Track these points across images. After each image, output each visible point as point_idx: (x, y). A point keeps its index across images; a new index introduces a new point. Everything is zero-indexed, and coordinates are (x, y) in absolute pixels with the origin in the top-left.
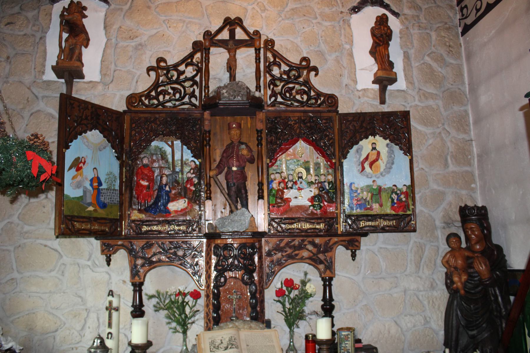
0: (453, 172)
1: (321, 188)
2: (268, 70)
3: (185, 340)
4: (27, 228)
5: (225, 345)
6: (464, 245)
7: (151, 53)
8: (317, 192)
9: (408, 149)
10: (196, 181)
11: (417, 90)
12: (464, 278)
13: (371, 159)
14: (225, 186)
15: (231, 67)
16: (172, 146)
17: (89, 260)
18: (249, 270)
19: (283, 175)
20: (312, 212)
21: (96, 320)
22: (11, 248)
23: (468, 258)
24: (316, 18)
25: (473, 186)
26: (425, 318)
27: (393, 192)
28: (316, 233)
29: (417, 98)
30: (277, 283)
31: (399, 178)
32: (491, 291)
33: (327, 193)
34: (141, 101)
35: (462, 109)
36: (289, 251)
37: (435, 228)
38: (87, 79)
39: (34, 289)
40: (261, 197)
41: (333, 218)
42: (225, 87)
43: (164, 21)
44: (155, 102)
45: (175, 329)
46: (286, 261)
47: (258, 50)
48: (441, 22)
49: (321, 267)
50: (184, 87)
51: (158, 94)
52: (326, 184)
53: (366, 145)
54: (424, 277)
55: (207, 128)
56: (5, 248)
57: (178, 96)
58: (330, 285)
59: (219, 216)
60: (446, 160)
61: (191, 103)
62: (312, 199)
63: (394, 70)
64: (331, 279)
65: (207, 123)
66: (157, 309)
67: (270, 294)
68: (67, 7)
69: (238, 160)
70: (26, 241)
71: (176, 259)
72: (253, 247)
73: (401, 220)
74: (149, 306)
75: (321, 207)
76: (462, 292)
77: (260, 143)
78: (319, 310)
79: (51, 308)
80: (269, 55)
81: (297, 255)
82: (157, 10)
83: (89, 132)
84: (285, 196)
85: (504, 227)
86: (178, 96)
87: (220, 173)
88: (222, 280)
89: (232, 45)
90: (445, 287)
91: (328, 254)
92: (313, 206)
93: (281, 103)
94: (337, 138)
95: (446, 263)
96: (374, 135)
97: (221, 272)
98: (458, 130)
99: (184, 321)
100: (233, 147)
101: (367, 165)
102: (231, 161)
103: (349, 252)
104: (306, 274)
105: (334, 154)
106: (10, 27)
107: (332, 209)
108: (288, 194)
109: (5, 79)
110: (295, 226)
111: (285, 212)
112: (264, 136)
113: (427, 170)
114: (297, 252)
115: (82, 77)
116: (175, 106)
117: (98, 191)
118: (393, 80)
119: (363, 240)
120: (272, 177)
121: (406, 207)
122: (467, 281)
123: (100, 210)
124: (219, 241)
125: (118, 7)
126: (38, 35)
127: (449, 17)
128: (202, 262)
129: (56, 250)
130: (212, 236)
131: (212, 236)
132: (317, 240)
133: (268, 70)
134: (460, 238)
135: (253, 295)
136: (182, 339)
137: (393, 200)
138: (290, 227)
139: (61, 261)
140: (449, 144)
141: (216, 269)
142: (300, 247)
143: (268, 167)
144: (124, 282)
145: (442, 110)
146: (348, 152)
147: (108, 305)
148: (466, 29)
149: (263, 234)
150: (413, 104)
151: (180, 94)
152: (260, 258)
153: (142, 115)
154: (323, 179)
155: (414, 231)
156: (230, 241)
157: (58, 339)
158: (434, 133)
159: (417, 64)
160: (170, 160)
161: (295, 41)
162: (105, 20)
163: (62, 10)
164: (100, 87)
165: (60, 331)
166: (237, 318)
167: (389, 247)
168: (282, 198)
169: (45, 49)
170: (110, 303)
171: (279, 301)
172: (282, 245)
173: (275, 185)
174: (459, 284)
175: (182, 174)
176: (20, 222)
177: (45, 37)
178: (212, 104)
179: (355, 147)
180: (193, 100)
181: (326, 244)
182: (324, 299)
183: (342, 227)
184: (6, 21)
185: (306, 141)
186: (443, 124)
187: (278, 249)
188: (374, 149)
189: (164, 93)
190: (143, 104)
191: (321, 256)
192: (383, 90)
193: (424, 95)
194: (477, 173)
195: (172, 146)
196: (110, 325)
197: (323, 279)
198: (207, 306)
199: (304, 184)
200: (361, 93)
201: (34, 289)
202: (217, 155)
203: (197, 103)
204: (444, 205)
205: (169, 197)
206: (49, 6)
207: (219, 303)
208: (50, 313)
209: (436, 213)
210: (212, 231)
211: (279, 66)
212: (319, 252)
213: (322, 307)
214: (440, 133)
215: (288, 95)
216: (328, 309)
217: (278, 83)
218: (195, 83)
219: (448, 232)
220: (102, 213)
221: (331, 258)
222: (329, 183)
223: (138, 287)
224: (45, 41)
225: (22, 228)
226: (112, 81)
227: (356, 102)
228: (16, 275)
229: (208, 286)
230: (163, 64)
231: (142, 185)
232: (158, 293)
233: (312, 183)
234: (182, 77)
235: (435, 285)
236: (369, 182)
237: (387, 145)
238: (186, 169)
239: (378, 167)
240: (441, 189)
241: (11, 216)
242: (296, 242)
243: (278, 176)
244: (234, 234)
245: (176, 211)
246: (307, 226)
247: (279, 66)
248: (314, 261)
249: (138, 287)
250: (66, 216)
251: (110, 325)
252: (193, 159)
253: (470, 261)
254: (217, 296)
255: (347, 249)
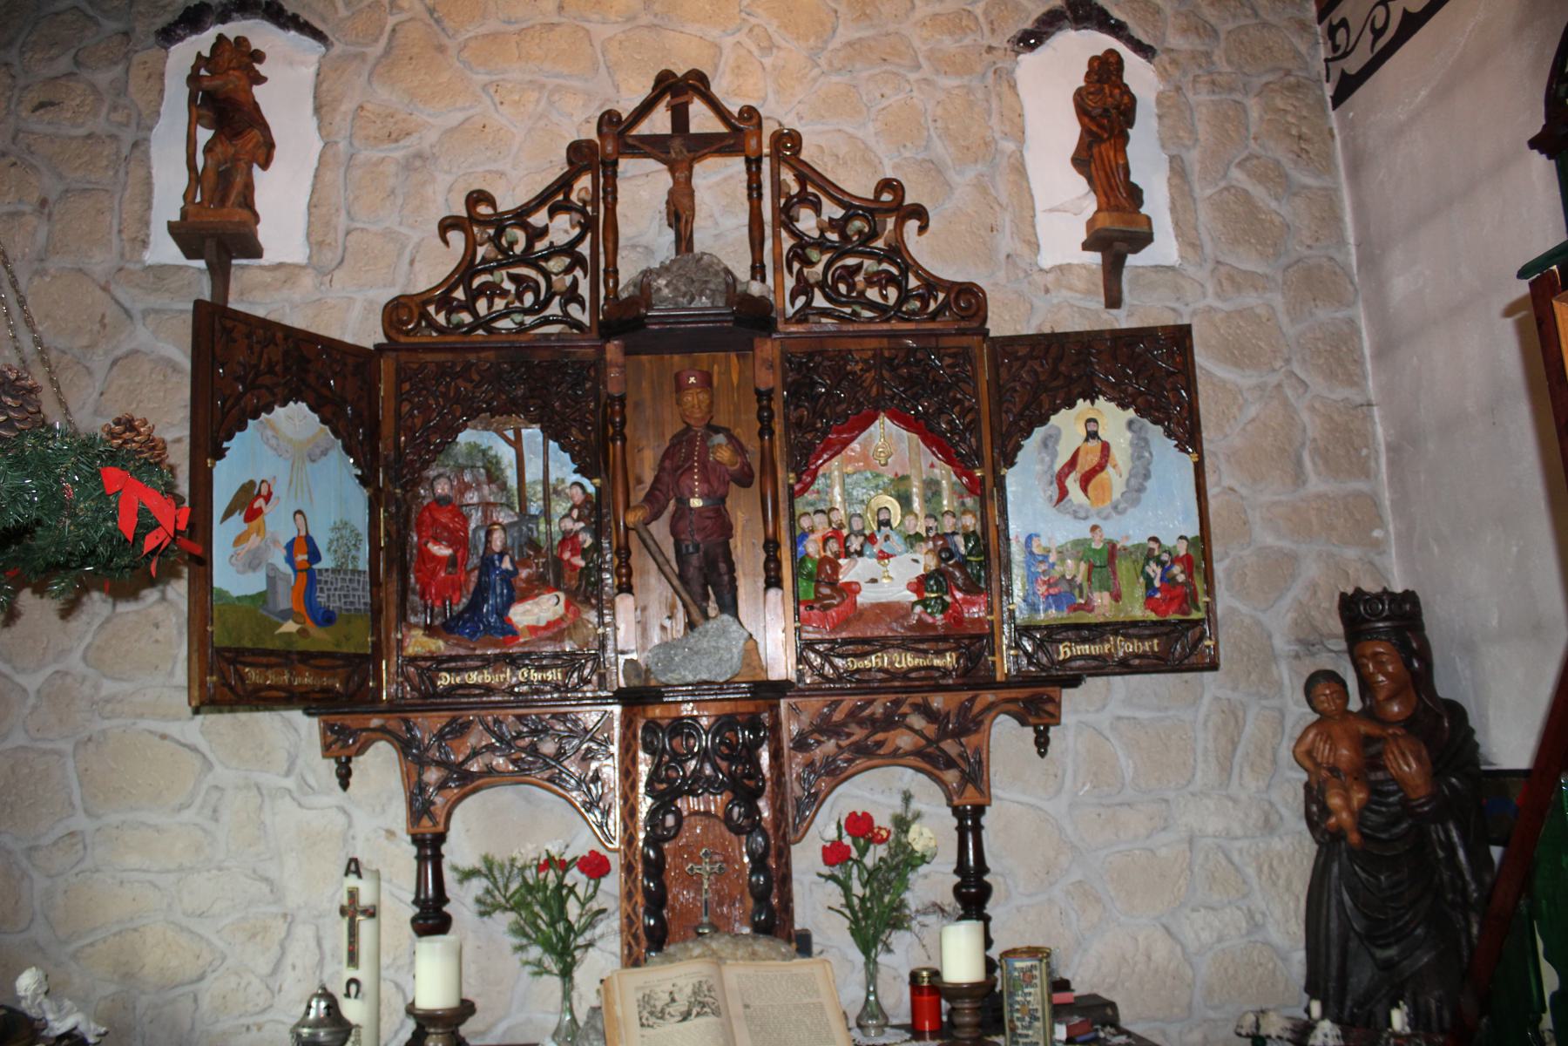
0: (1319, 496)
1: (945, 552)
2: (786, 218)
3: (567, 996)
4: (109, 687)
5: (681, 1005)
6: (1355, 704)
7: (450, 179)
8: (932, 563)
9: (1188, 435)
10: (587, 540)
11: (1209, 266)
12: (1359, 797)
13: (1085, 464)
14: (671, 553)
15: (680, 213)
16: (517, 443)
17: (288, 773)
18: (745, 790)
19: (835, 517)
20: (920, 620)
21: (313, 944)
22: (67, 746)
23: (1368, 740)
24: (918, 67)
25: (1377, 533)
26: (1251, 915)
27: (1149, 557)
28: (932, 681)
29: (1210, 289)
30: (825, 826)
31: (1163, 517)
32: (1436, 832)
33: (962, 564)
34: (424, 315)
35: (1339, 315)
36: (858, 734)
37: (1274, 657)
38: (269, 258)
39: (133, 860)
40: (773, 581)
41: (980, 637)
42: (664, 269)
43: (485, 87)
44: (466, 318)
45: (539, 963)
46: (849, 761)
47: (753, 164)
48: (1273, 70)
49: (951, 776)
50: (547, 275)
51: (473, 295)
52: (959, 540)
53: (1068, 425)
54: (1243, 796)
55: (614, 389)
56: (49, 746)
57: (529, 299)
58: (977, 829)
59: (656, 638)
60: (1299, 463)
61: (566, 319)
62: (920, 585)
63: (1143, 210)
64: (979, 810)
65: (613, 373)
66: (486, 908)
67: (806, 859)
68: (206, 53)
69: (705, 479)
70: (106, 724)
71: (536, 760)
72: (754, 724)
73: (1175, 638)
74: (462, 901)
75: (945, 607)
76: (1354, 838)
77: (766, 429)
78: (949, 900)
79: (184, 913)
80: (787, 176)
81: (880, 744)
82: (465, 54)
83: (278, 410)
84: (844, 578)
85: (1469, 648)
86: (529, 299)
87: (656, 516)
88: (670, 820)
89: (680, 151)
90: (1303, 826)
91: (971, 741)
92: (923, 602)
93: (823, 312)
94: (985, 408)
95: (1305, 756)
96: (1091, 396)
97: (665, 799)
98: (1331, 375)
99: (564, 940)
100: (691, 442)
101: (1072, 483)
102: (685, 482)
103: (1029, 733)
104: (907, 798)
105: (978, 454)
106: (47, 115)
107: (976, 612)
108: (851, 571)
109: (36, 265)
110: (872, 661)
111: (844, 622)
112: (777, 406)
113: (1243, 491)
114: (879, 736)
115: (255, 251)
116: (522, 329)
117: (309, 578)
118: (1142, 239)
119: (1068, 697)
120: (805, 523)
121: (1187, 599)
122: (1366, 806)
123: (316, 632)
124: (657, 711)
125: (352, 49)
126: (128, 136)
127: (1297, 54)
128: (610, 770)
129: (194, 749)
130: (638, 697)
131: (638, 697)
132: (937, 702)
133: (786, 218)
134: (1343, 684)
135: (759, 863)
136: (559, 994)
137: (1149, 580)
138: (859, 664)
139: (210, 779)
140: (1305, 416)
141: (650, 791)
142: (890, 722)
143: (792, 495)
144: (391, 834)
145: (1284, 320)
146: (1019, 447)
147: (345, 902)
148: (1346, 88)
149: (782, 688)
150: (1201, 305)
151: (537, 293)
152: (776, 756)
153: (429, 357)
154: (948, 525)
155: (1214, 666)
156: (687, 709)
157: (206, 1002)
158: (1261, 387)
159: (1209, 192)
160: (512, 482)
161: (860, 134)
162: (317, 87)
163: (192, 61)
164: (308, 280)
165: (210, 977)
166: (715, 929)
167: (1143, 715)
168: (833, 584)
169: (149, 176)
170: (353, 894)
171: (832, 878)
172: (837, 717)
173: (812, 547)
174: (1344, 815)
175: (548, 522)
176: (90, 672)
177: (147, 140)
178: (626, 320)
179: (1039, 433)
180: (574, 310)
181: (964, 710)
182: (961, 868)
183: (1006, 663)
184: (34, 96)
185: (899, 418)
186: (1288, 361)
187: (825, 728)
188: (1092, 435)
189: (492, 291)
190: (432, 324)
191: (950, 746)
192: (1113, 269)
193: (1231, 278)
194: (1386, 497)
195: (517, 443)
196: (353, 958)
197: (957, 812)
198: (629, 895)
199: (896, 543)
200: (1051, 277)
201: (133, 860)
202: (647, 467)
203: (585, 319)
204: (1297, 591)
205: (511, 588)
206: (157, 52)
207: (662, 887)
208: (182, 929)
209: (1272, 616)
210: (635, 682)
211: (817, 207)
212: (944, 734)
213: (957, 890)
214: (1279, 386)
215: (843, 288)
216: (973, 896)
217: (814, 255)
218: (578, 261)
219: (1309, 667)
220: (322, 638)
221: (978, 751)
222: (967, 537)
223: (430, 847)
224: (146, 162)
225: (97, 687)
226: (342, 261)
227: (1037, 303)
228: (80, 822)
229: (630, 840)
230: (484, 210)
231: (434, 558)
232: (488, 862)
233: (917, 537)
234: (540, 246)
235: (1274, 819)
236: (1081, 530)
237: (1130, 424)
238: (560, 508)
239: (1106, 488)
240: (1286, 544)
241: (63, 653)
242: (878, 709)
243: (820, 520)
244: (699, 689)
245: (533, 629)
246: (908, 661)
247: (817, 207)
248: (930, 760)
249: (430, 847)
250: (219, 651)
251: (353, 958)
252: (577, 477)
253: (1373, 750)
254: (655, 869)
255: (1023, 723)
